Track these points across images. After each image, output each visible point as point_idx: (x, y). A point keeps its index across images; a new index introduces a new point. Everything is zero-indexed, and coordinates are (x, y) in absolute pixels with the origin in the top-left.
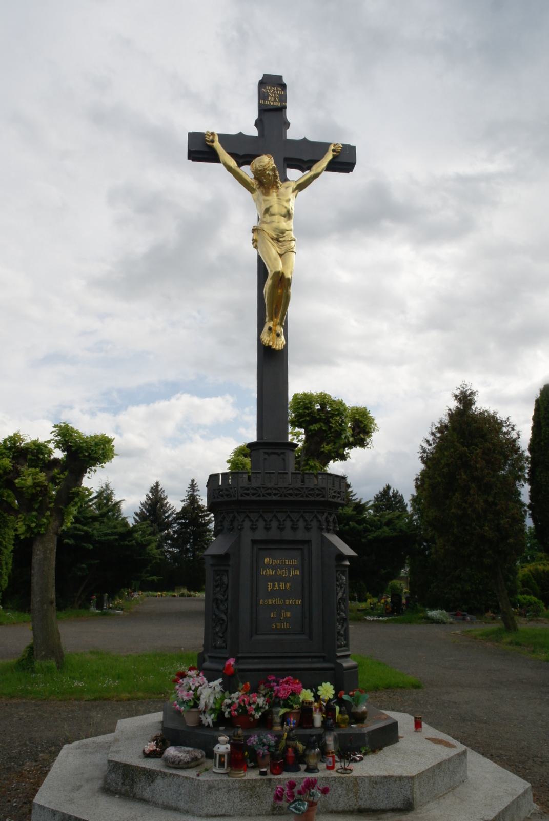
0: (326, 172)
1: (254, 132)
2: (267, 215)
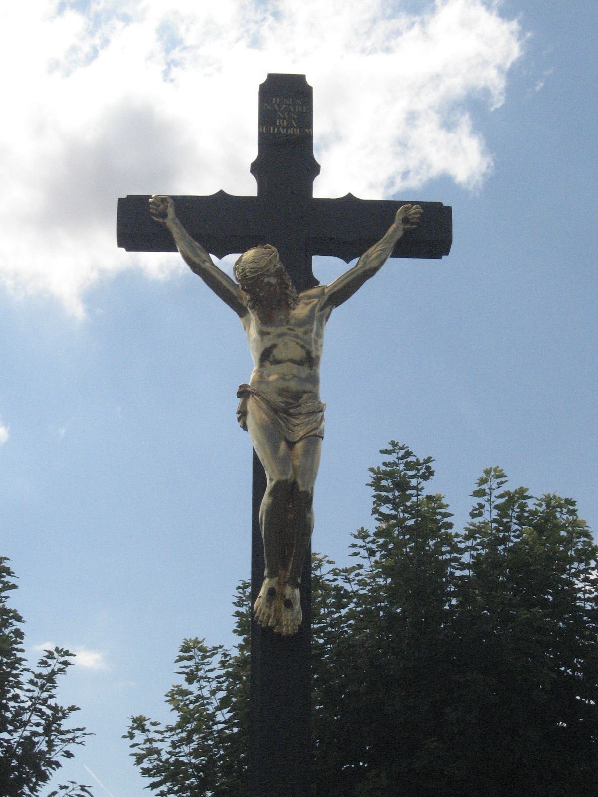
0: (391, 258)
1: (248, 187)
2: (267, 363)
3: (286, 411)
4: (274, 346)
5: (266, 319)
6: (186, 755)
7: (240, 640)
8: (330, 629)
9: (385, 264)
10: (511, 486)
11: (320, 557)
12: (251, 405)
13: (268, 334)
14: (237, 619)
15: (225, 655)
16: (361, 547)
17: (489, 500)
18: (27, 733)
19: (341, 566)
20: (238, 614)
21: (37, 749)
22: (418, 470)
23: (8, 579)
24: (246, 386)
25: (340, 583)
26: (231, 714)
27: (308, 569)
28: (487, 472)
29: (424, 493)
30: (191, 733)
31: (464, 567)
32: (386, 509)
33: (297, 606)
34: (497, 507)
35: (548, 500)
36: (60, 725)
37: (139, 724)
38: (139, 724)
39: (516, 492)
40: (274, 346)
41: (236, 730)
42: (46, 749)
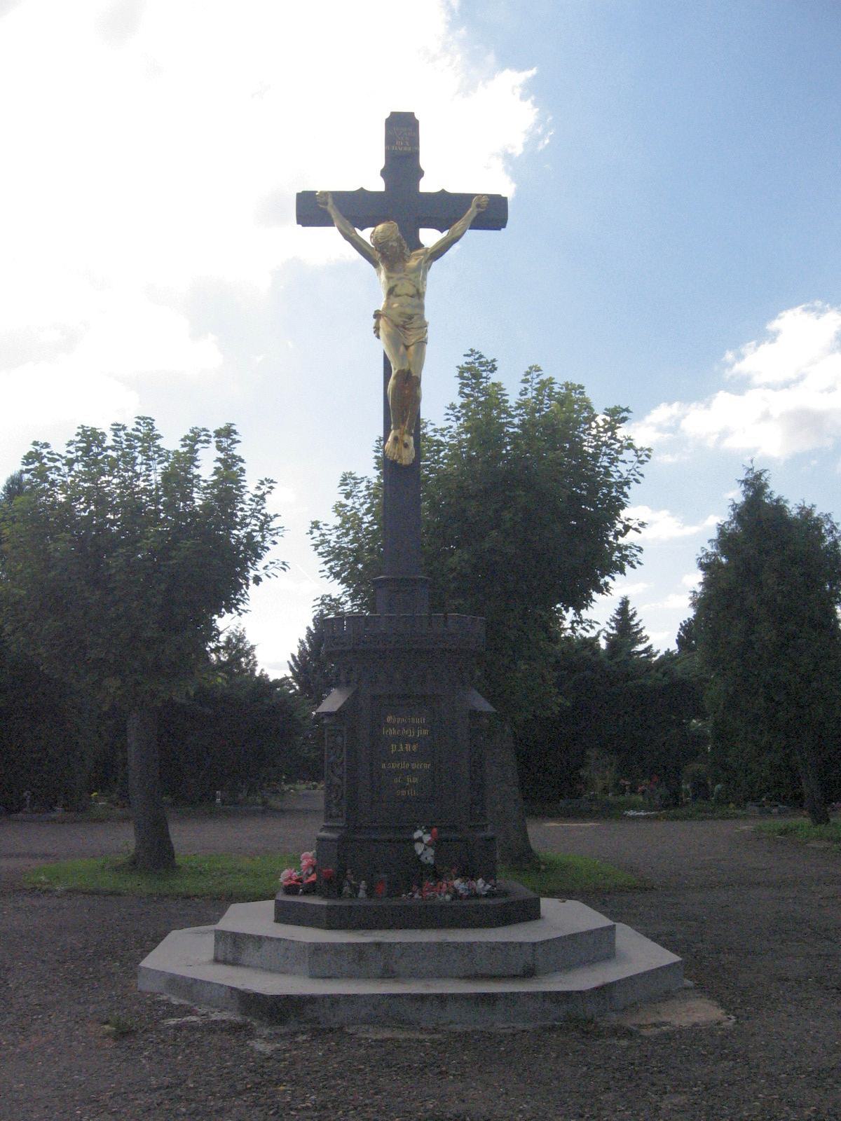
2: (391, 297)
3: (403, 327)
4: (396, 286)
5: (390, 269)
6: (345, 543)
7: (377, 473)
8: (433, 465)
9: (465, 235)
10: (544, 377)
11: (426, 421)
12: (382, 322)
13: (392, 278)
14: (375, 460)
15: (369, 482)
16: (451, 415)
17: (531, 386)
18: (249, 530)
19: (439, 427)
20: (376, 457)
21: (255, 540)
22: (487, 367)
23: (234, 437)
24: (379, 311)
25: (438, 437)
26: (373, 518)
27: (418, 429)
28: (531, 368)
29: (491, 381)
30: (348, 530)
31: (514, 426)
32: (467, 391)
33: (412, 447)
34: (535, 389)
35: (567, 385)
36: (269, 525)
37: (316, 525)
38: (316, 525)
39: (547, 380)
40: (396, 286)
41: (375, 527)
42: (260, 540)
